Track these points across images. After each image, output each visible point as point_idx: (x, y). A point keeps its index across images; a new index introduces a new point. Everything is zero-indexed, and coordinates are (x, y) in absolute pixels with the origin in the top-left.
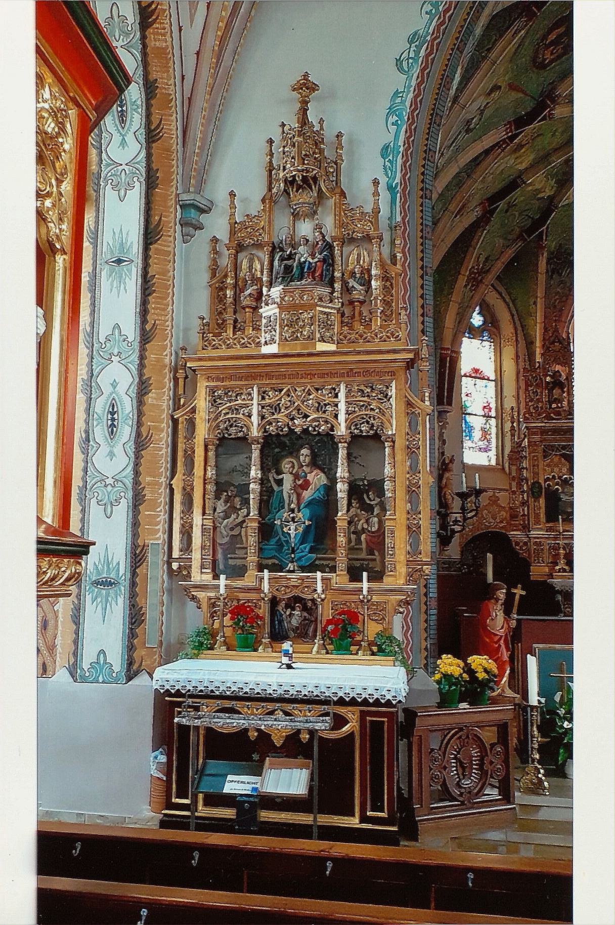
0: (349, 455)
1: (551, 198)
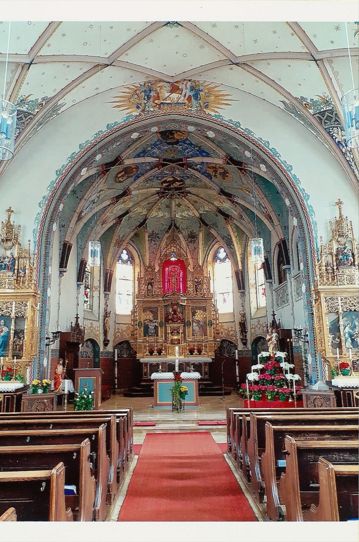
0: (15, 322)
1: (146, 215)
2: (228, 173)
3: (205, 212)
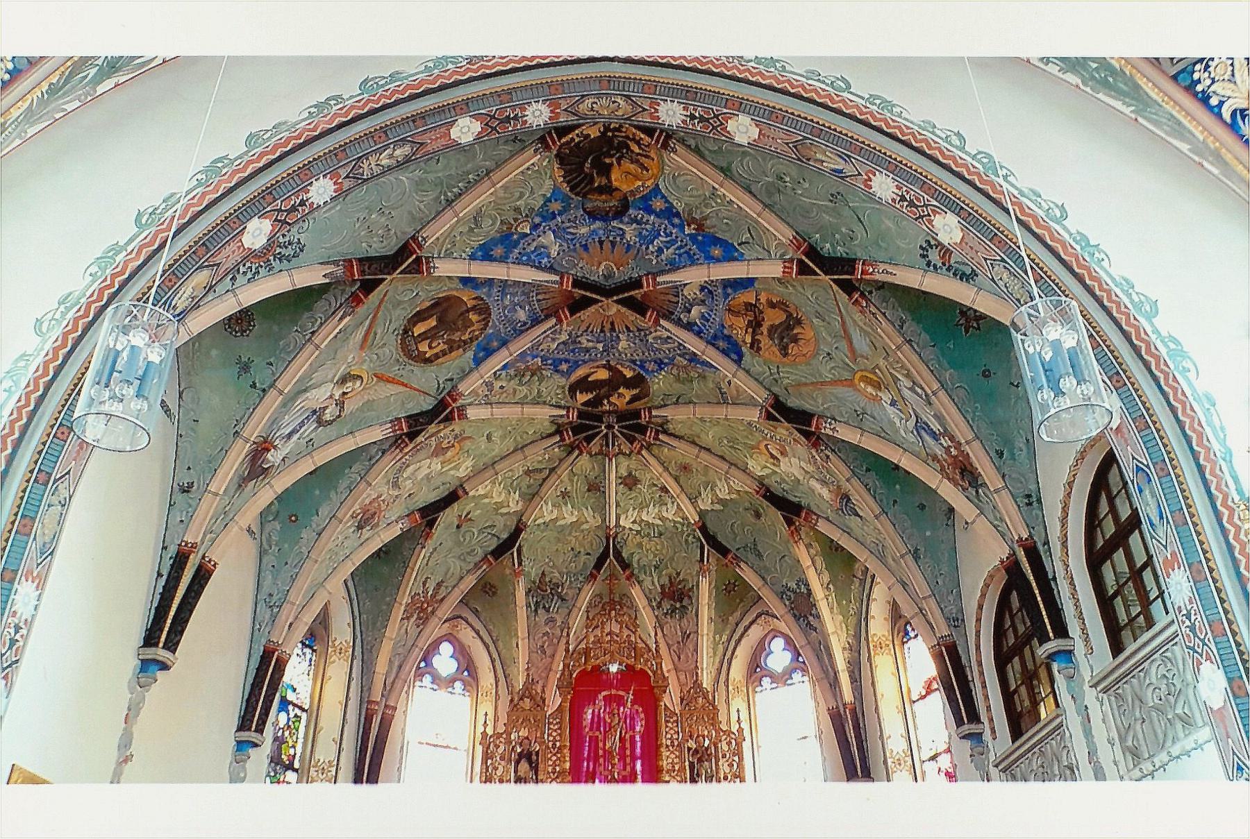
1: (520, 515)
2: (799, 322)
3: (717, 507)
